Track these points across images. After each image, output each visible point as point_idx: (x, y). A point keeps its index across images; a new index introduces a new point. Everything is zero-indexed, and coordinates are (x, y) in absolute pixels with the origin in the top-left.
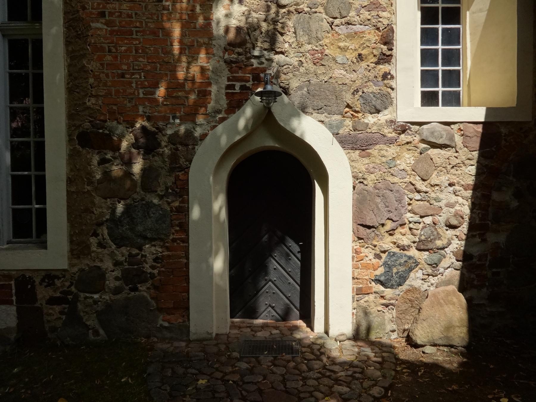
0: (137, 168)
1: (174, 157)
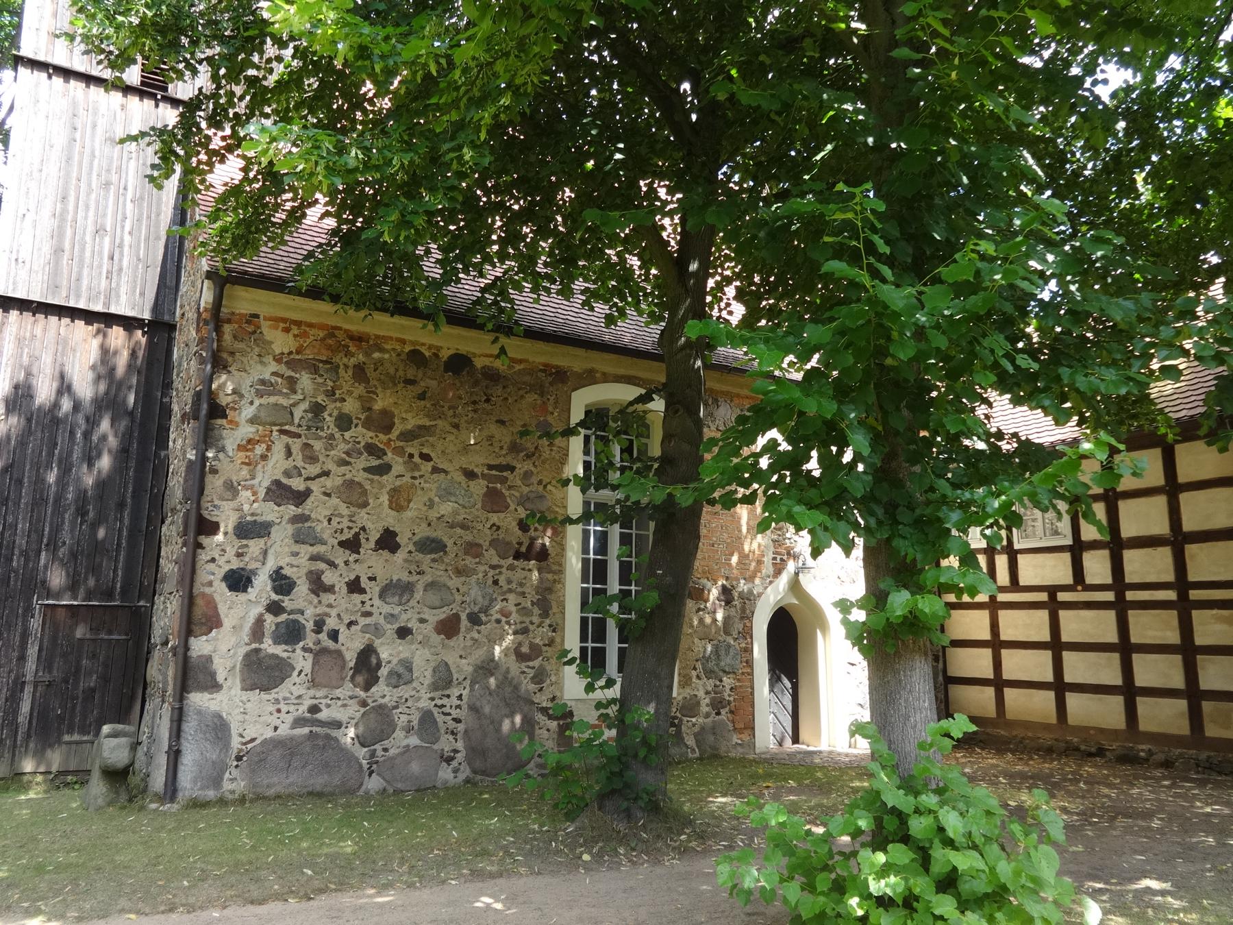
0: (720, 616)
1: (743, 610)
